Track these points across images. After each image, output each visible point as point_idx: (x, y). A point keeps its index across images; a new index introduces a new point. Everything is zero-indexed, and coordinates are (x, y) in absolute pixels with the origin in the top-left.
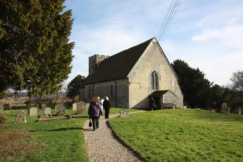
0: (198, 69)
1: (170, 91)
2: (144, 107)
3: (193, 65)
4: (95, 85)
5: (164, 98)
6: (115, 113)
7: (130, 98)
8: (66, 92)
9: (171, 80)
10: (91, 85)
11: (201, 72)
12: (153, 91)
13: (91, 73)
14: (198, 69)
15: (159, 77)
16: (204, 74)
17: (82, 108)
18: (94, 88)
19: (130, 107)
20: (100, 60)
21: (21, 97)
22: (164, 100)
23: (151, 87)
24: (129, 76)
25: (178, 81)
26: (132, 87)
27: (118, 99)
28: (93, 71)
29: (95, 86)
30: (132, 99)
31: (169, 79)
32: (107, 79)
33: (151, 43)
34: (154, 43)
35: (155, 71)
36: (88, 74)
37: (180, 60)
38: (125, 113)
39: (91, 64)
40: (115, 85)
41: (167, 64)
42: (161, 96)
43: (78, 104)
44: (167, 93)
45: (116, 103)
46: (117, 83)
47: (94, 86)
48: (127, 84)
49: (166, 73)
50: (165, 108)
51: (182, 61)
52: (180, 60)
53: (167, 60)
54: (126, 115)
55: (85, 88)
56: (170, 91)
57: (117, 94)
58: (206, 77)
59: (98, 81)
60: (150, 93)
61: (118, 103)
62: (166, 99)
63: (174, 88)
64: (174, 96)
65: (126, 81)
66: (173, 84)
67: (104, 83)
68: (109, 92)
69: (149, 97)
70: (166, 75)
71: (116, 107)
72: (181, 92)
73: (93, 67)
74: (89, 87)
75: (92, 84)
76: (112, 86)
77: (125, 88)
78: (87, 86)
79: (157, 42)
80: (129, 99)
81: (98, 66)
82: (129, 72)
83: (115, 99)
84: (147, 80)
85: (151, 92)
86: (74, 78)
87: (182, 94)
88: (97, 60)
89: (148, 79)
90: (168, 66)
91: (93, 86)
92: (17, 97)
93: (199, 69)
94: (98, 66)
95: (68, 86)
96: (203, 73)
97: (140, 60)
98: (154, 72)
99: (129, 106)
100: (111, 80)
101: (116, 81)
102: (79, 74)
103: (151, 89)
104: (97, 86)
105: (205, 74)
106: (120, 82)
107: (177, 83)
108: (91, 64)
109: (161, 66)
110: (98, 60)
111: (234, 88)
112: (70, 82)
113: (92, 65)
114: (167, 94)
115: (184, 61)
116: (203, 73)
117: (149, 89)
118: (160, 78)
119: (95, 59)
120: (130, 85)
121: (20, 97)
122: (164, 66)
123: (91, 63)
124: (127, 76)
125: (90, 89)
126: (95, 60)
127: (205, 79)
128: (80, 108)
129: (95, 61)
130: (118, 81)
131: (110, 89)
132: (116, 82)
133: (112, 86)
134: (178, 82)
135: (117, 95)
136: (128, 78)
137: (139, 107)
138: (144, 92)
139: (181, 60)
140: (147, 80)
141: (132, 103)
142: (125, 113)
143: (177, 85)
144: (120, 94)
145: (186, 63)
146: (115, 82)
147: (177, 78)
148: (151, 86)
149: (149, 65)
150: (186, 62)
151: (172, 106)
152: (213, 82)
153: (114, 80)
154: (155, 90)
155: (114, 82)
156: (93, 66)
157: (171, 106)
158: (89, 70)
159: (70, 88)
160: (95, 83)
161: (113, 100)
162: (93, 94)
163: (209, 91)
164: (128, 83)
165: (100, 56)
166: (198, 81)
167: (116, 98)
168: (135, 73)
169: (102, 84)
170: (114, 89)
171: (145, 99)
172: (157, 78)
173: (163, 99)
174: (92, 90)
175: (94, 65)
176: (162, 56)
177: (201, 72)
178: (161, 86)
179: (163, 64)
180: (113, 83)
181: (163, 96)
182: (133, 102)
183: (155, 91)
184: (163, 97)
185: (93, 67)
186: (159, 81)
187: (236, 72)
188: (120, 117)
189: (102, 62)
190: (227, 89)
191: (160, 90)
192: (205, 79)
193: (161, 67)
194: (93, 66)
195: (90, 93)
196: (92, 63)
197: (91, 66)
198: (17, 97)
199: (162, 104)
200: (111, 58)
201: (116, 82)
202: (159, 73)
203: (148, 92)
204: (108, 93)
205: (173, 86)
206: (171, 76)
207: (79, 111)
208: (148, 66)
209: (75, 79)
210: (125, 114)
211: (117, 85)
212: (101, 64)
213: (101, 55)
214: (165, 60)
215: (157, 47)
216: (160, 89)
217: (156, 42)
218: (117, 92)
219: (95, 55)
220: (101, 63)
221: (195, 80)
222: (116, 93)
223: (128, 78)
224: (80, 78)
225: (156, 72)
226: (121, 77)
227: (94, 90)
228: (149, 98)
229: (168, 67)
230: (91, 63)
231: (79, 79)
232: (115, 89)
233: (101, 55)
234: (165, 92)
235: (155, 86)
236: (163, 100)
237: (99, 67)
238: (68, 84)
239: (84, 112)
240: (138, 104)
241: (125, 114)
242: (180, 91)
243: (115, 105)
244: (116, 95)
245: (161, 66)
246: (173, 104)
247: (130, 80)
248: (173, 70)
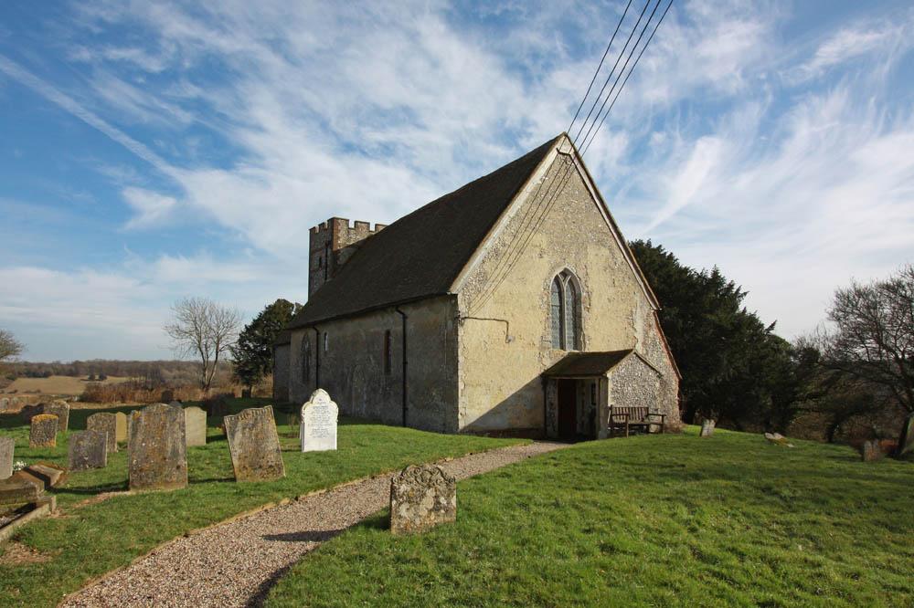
0: (715, 274)
1: (637, 356)
2: (524, 423)
3: (694, 259)
4: (323, 330)
5: (610, 385)
6: (379, 472)
7: (461, 386)
8: (233, 361)
9: (632, 311)
10: (312, 333)
11: (731, 286)
12: (560, 354)
13: (316, 287)
14: (715, 274)
15: (584, 294)
16: (741, 292)
17: (162, 450)
18: (322, 341)
19: (462, 424)
20: (349, 240)
21: (108, 377)
22: (613, 392)
23: (550, 338)
24: (457, 288)
25: (660, 315)
26: (469, 336)
27: (410, 390)
28: (324, 281)
29: (326, 334)
30: (469, 390)
31: (623, 306)
32: (370, 306)
33: (552, 156)
34: (564, 154)
35: (565, 269)
36: (307, 300)
37: (645, 242)
38: (430, 493)
39: (317, 255)
40: (401, 327)
41: (615, 246)
42: (596, 375)
43: (138, 420)
44: (624, 362)
45: (404, 405)
46: (408, 320)
47: (322, 336)
48: (450, 322)
49: (611, 282)
50: (618, 431)
51: (654, 246)
52: (645, 242)
53: (615, 227)
54: (437, 507)
55: (289, 343)
56: (637, 356)
57: (409, 367)
58: (747, 305)
59: (334, 315)
60: (548, 363)
61: (410, 406)
62: (620, 390)
63: (644, 344)
64: (655, 378)
65: (445, 309)
66: (639, 325)
67: (357, 322)
68: (374, 357)
69: (545, 377)
70: (612, 290)
71: (404, 425)
72: (670, 358)
73: (323, 264)
74: (305, 340)
75: (313, 325)
76: (388, 333)
77: (442, 342)
78: (297, 337)
79: (576, 153)
80: (456, 387)
81: (342, 260)
82: (460, 271)
83: (401, 384)
84: (534, 307)
85: (551, 358)
86: (264, 309)
87: (675, 369)
88: (339, 238)
89: (537, 302)
90: (617, 251)
91: (318, 334)
92: (97, 377)
93: (722, 274)
94: (342, 260)
95: (241, 341)
96: (738, 290)
97: (505, 220)
98: (565, 273)
99: (458, 420)
100: (383, 309)
101: (402, 311)
102: (282, 297)
103: (550, 345)
104: (330, 334)
105: (745, 294)
106: (418, 317)
107: (653, 321)
108: (317, 255)
109: (591, 250)
110: (342, 240)
111: (843, 343)
112: (249, 323)
113: (320, 259)
114: (623, 366)
115: (660, 246)
116: (738, 290)
117: (543, 348)
118: (587, 300)
119: (332, 236)
120: (462, 325)
121: (106, 378)
122: (605, 252)
123: (317, 251)
124: (452, 289)
125: (307, 346)
126: (332, 239)
127: (744, 311)
128: (153, 444)
129: (330, 244)
130: (411, 312)
131: (382, 347)
132: (405, 318)
133: (388, 333)
134: (656, 320)
135: (409, 373)
136: (456, 296)
137: (500, 422)
138: (522, 357)
139: (649, 244)
140: (534, 307)
141: (473, 406)
142: (430, 493)
143: (655, 333)
144: (419, 367)
145: (667, 255)
146: (401, 316)
147: (655, 303)
148: (551, 335)
149: (544, 246)
150: (667, 250)
151: (646, 421)
152: (773, 325)
153: (397, 306)
154: (569, 350)
155: (398, 317)
156: (324, 261)
157: (643, 420)
158: (310, 278)
159: (249, 347)
160: (325, 322)
161: (392, 393)
162: (318, 366)
163: (763, 358)
164: (457, 319)
165: (352, 225)
166: (719, 317)
167: (404, 383)
168: (483, 278)
169: (350, 327)
170: (396, 346)
171: (528, 387)
172: (577, 301)
173: (610, 390)
174: (314, 350)
175: (326, 256)
176: (595, 210)
177: (731, 286)
178: (592, 336)
179: (600, 243)
180: (391, 321)
181: (609, 375)
182: (474, 404)
183: (571, 356)
184: (607, 379)
185: (323, 264)
186: (584, 313)
187: (846, 286)
188: (383, 534)
189: (360, 247)
190: (809, 354)
191: (587, 351)
192: (744, 311)
193: (591, 257)
194: (324, 261)
195: (308, 364)
196: (320, 250)
197: (316, 263)
198: (97, 377)
199: (602, 413)
200: (388, 229)
201: (405, 318)
202: (583, 280)
203: (541, 358)
204: (373, 361)
205: (640, 335)
206: (632, 295)
207: (146, 466)
208: (538, 250)
209: (266, 313)
210: (428, 502)
211: (410, 327)
212: (355, 253)
213: (356, 222)
214: (606, 230)
215: (575, 173)
216: (587, 346)
217: (572, 153)
218: (408, 360)
219: (332, 221)
220: (352, 250)
221: (709, 316)
222: (405, 363)
223: (456, 296)
224: (284, 312)
225: (572, 274)
226: (426, 293)
227: (322, 353)
228: (542, 383)
229: (620, 257)
230: (317, 251)
231: (281, 312)
232: (401, 346)
233: (356, 222)
234: (615, 358)
235: (569, 333)
236: (609, 392)
237: (346, 264)
238: (239, 332)
239: (176, 473)
240: (494, 412)
241: (428, 502)
242: (665, 354)
243: (399, 417)
244: (401, 371)
245: (591, 250)
246: (650, 412)
247: (462, 307)
248: (638, 271)
